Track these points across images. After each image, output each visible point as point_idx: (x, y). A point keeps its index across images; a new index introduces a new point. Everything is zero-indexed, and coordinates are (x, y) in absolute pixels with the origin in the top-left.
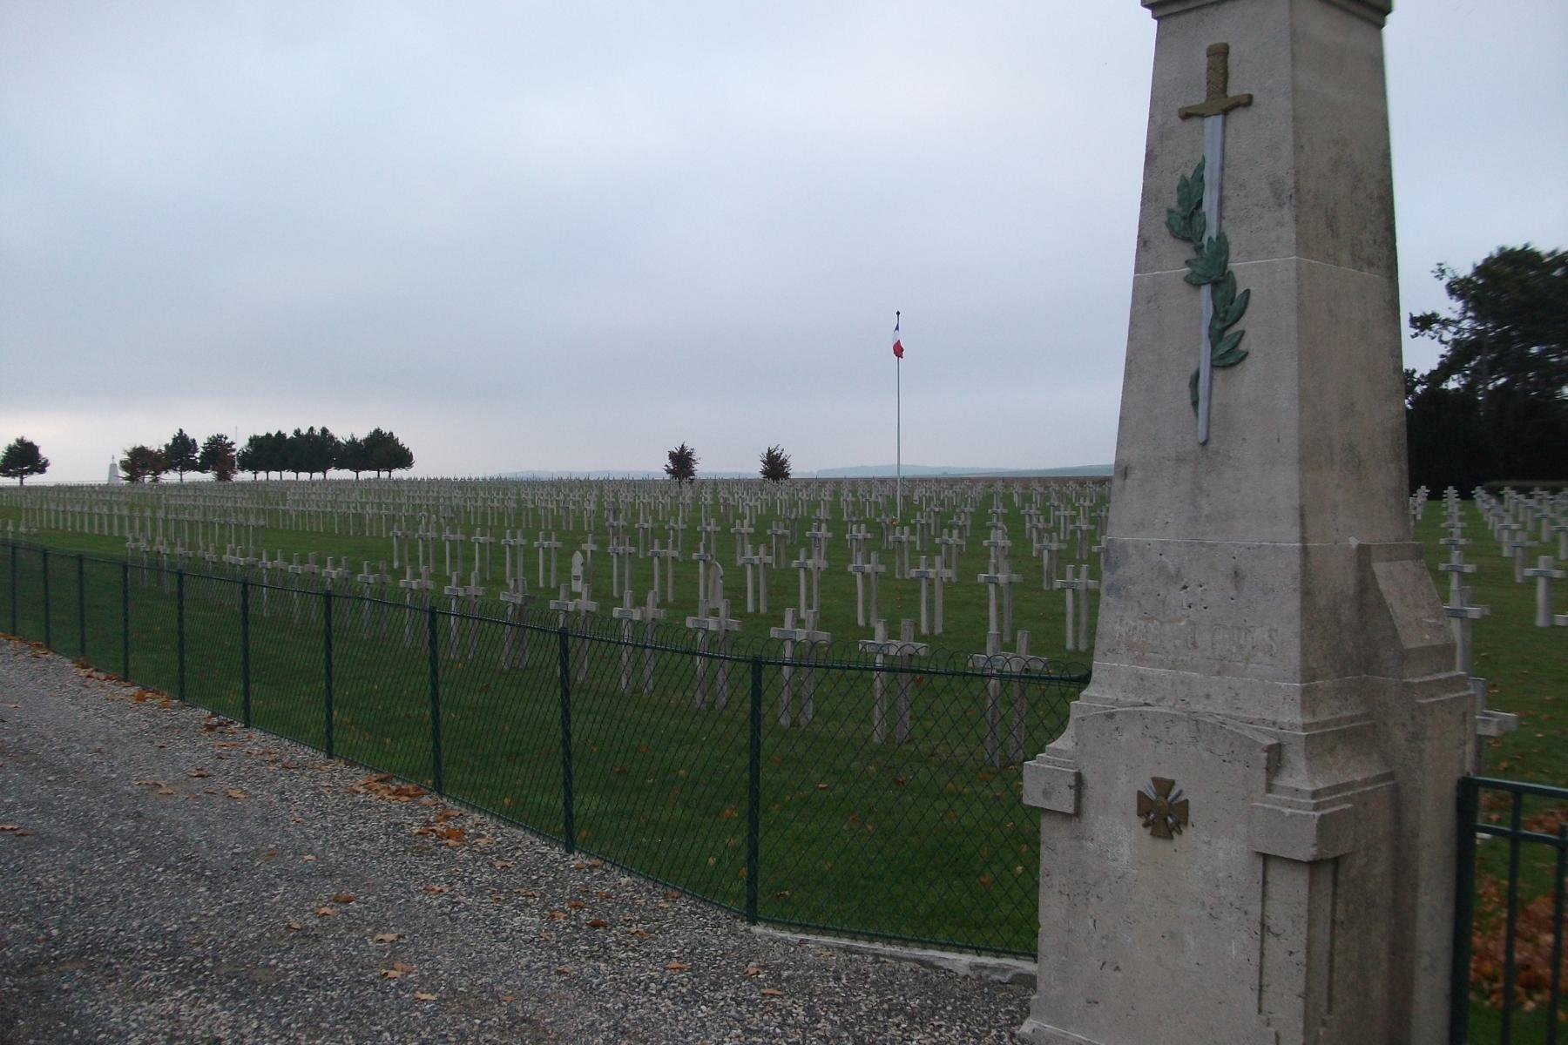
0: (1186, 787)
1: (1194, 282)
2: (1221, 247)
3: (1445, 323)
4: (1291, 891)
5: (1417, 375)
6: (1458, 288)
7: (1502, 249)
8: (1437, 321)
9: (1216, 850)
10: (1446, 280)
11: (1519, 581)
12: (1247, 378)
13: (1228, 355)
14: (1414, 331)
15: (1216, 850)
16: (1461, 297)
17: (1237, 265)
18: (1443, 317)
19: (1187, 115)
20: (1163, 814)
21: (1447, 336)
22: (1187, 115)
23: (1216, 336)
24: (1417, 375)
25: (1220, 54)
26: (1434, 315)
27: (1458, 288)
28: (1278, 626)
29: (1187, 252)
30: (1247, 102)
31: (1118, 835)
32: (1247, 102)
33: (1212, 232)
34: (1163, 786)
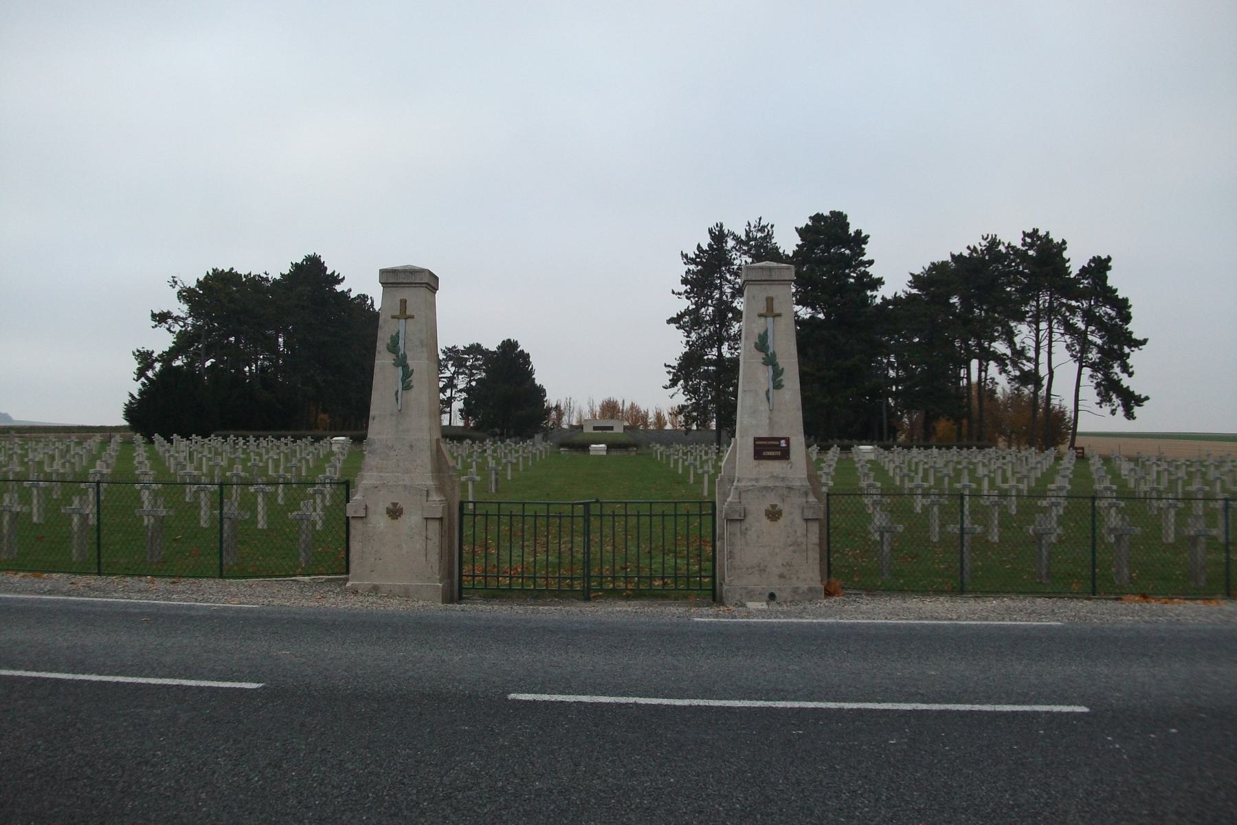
0: (401, 504)
1: (396, 365)
2: (405, 356)
3: (177, 319)
4: (434, 526)
5: (155, 355)
6: (187, 295)
7: (610, 408)
8: (171, 318)
9: (412, 519)
10: (177, 289)
11: (565, 426)
12: (413, 393)
13: (407, 387)
14: (154, 323)
15: (412, 519)
16: (187, 302)
17: (409, 362)
18: (175, 315)
19: (393, 317)
20: (395, 512)
21: (177, 328)
22: (393, 317)
23: (403, 381)
24: (155, 355)
25: (404, 303)
26: (169, 312)
27: (187, 295)
28: (425, 460)
29: (394, 356)
30: (412, 317)
31: (380, 521)
32: (412, 317)
33: (402, 352)
34: (395, 505)
